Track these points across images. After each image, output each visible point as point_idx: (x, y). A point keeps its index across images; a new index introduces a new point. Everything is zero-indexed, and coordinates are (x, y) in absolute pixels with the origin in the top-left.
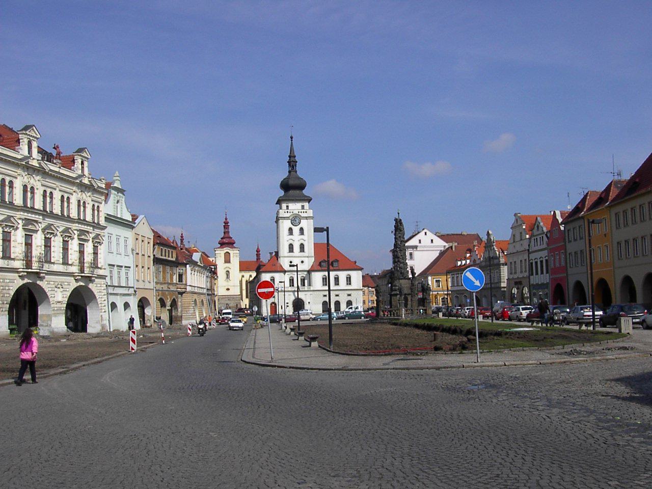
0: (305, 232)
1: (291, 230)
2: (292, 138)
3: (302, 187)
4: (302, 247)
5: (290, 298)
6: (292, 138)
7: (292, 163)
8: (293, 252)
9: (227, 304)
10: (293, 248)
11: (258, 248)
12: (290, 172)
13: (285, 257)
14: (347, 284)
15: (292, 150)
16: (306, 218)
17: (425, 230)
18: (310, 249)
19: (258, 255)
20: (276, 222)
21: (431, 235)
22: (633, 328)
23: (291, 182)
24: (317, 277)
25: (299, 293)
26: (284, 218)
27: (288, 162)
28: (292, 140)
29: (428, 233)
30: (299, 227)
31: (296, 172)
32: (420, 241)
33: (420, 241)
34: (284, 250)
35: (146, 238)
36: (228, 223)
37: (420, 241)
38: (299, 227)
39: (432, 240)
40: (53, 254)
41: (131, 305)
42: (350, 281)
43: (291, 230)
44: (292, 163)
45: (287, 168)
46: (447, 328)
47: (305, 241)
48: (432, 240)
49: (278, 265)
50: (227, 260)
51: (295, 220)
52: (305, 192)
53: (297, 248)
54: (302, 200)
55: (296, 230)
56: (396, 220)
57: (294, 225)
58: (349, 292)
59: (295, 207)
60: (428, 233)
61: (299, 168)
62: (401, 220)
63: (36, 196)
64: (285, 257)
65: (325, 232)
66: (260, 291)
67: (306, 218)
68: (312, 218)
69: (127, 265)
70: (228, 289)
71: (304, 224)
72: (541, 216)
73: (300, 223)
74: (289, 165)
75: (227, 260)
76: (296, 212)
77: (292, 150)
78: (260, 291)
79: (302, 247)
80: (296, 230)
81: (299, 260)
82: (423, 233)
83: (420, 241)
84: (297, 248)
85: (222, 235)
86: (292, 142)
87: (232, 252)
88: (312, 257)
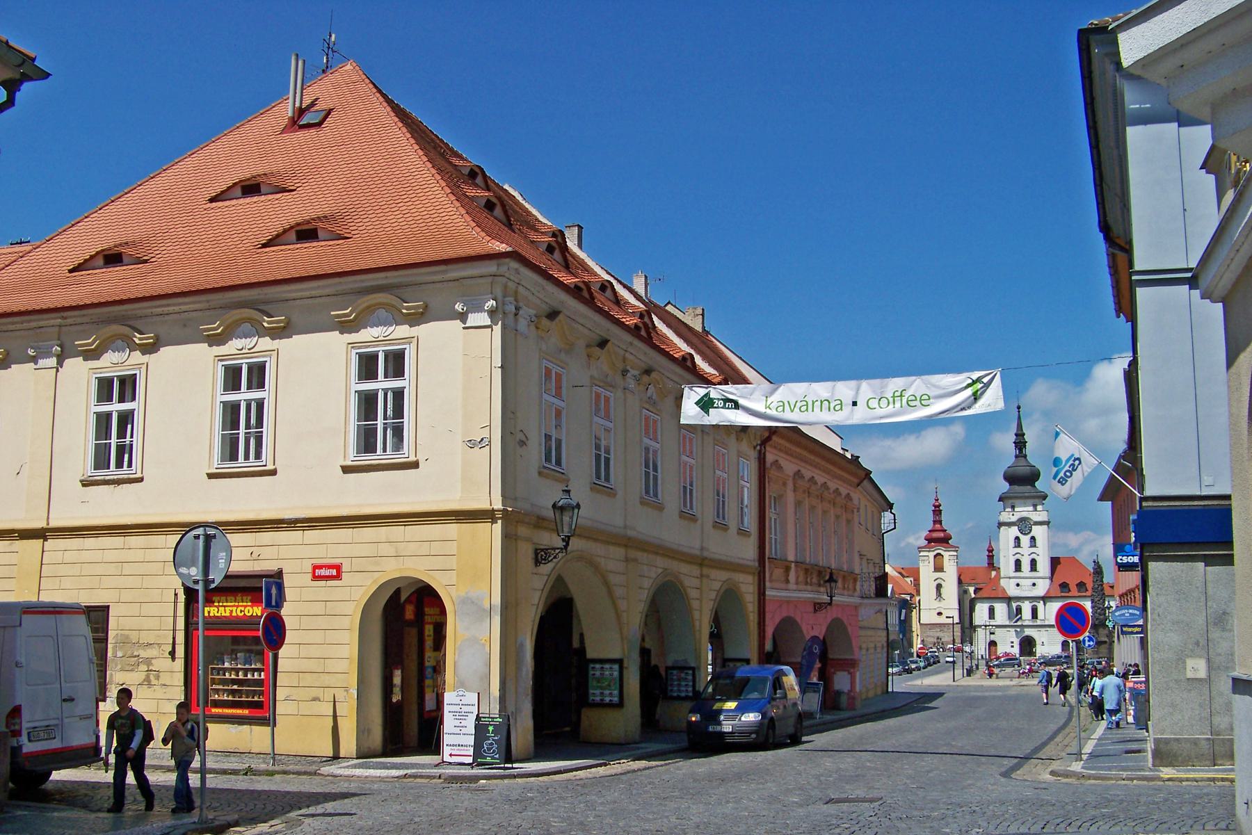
1: (1017, 538)
2: (1019, 408)
4: (1033, 564)
6: (1019, 408)
12: (1016, 457)
16: (1037, 523)
18: (1044, 567)
19: (991, 557)
22: (110, 381)
23: (1023, 470)
25: (269, 750)
26: (1010, 524)
31: (1025, 456)
34: (1006, 564)
43: (1017, 538)
50: (939, 568)
51: (1024, 525)
53: (1026, 566)
54: (1116, 104)
55: (1025, 540)
59: (1024, 511)
61: (1029, 449)
67: (1037, 523)
68: (1047, 523)
69: (612, 462)
70: (940, 614)
75: (939, 568)
76: (1025, 515)
79: (1033, 564)
80: (1025, 540)
81: (1030, 582)
84: (1026, 566)
85: (930, 526)
87: (946, 555)
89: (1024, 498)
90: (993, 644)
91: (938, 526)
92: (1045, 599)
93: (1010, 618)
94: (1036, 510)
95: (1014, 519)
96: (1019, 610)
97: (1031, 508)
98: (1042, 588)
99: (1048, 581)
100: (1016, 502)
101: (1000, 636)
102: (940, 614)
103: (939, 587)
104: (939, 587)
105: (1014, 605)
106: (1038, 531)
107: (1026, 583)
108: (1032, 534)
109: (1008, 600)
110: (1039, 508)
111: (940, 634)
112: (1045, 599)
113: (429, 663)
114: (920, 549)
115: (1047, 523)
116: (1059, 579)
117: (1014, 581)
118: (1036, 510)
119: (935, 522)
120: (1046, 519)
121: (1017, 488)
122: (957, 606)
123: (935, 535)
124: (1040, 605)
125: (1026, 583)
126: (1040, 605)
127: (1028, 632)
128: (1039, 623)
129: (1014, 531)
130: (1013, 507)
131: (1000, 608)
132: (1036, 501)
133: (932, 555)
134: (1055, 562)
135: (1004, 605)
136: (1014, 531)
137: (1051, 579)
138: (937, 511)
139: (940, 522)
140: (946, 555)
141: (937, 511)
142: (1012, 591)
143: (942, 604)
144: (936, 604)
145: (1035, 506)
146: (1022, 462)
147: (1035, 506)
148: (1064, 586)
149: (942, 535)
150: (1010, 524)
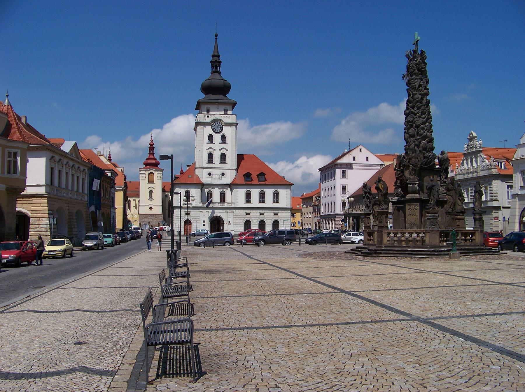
0: (228, 140)
1: (211, 137)
2: (216, 35)
3: (224, 89)
4: (223, 157)
5: (206, 215)
6: (216, 35)
7: (216, 64)
9: (149, 223)
11: (182, 170)
13: (203, 168)
15: (216, 49)
17: (361, 147)
18: (231, 160)
20: (194, 129)
21: (366, 153)
23: (217, 82)
24: (241, 193)
27: (211, 62)
28: (216, 39)
31: (219, 73)
32: (354, 159)
33: (354, 159)
34: (201, 159)
36: (153, 144)
37: (354, 158)
39: (367, 158)
43: (211, 137)
44: (216, 64)
45: (209, 68)
46: (54, 221)
47: (227, 150)
48: (367, 158)
49: (195, 177)
50: (151, 181)
52: (230, 96)
53: (217, 158)
55: (217, 138)
57: (214, 132)
59: (217, 114)
60: (363, 149)
61: (222, 69)
62: (422, 52)
64: (203, 168)
70: (151, 208)
73: (222, 130)
74: (212, 66)
75: (151, 181)
76: (218, 117)
77: (216, 49)
79: (223, 157)
80: (217, 138)
81: (220, 172)
82: (358, 149)
83: (354, 158)
84: (217, 158)
86: (216, 43)
87: (156, 173)
89: (218, 104)
90: (188, 223)
91: (152, 156)
92: (232, 186)
93: (202, 201)
94: (226, 113)
95: (208, 120)
96: (210, 195)
97: (223, 113)
98: (230, 177)
99: (234, 172)
100: (211, 107)
101: (194, 216)
102: (151, 208)
103: (151, 192)
104: (151, 192)
105: (206, 190)
106: (227, 131)
107: (216, 173)
108: (223, 132)
109: (202, 186)
110: (229, 112)
111: (151, 221)
112: (232, 186)
113: (188, 228)
114: (140, 170)
116: (244, 170)
117: (206, 171)
118: (226, 113)
119: (150, 154)
121: (211, 96)
122: (161, 204)
123: (150, 161)
124: (228, 191)
125: (216, 173)
126: (228, 191)
127: (218, 213)
128: (226, 205)
129: (208, 130)
130: (208, 112)
131: (195, 192)
132: (227, 107)
133: (147, 173)
134: (240, 158)
135: (198, 190)
136: (208, 130)
137: (237, 170)
139: (153, 154)
140: (156, 173)
142: (205, 179)
143: (153, 203)
144: (149, 202)
145: (226, 111)
146: (216, 76)
147: (226, 111)
148: (248, 176)
149: (154, 161)
150: (205, 124)
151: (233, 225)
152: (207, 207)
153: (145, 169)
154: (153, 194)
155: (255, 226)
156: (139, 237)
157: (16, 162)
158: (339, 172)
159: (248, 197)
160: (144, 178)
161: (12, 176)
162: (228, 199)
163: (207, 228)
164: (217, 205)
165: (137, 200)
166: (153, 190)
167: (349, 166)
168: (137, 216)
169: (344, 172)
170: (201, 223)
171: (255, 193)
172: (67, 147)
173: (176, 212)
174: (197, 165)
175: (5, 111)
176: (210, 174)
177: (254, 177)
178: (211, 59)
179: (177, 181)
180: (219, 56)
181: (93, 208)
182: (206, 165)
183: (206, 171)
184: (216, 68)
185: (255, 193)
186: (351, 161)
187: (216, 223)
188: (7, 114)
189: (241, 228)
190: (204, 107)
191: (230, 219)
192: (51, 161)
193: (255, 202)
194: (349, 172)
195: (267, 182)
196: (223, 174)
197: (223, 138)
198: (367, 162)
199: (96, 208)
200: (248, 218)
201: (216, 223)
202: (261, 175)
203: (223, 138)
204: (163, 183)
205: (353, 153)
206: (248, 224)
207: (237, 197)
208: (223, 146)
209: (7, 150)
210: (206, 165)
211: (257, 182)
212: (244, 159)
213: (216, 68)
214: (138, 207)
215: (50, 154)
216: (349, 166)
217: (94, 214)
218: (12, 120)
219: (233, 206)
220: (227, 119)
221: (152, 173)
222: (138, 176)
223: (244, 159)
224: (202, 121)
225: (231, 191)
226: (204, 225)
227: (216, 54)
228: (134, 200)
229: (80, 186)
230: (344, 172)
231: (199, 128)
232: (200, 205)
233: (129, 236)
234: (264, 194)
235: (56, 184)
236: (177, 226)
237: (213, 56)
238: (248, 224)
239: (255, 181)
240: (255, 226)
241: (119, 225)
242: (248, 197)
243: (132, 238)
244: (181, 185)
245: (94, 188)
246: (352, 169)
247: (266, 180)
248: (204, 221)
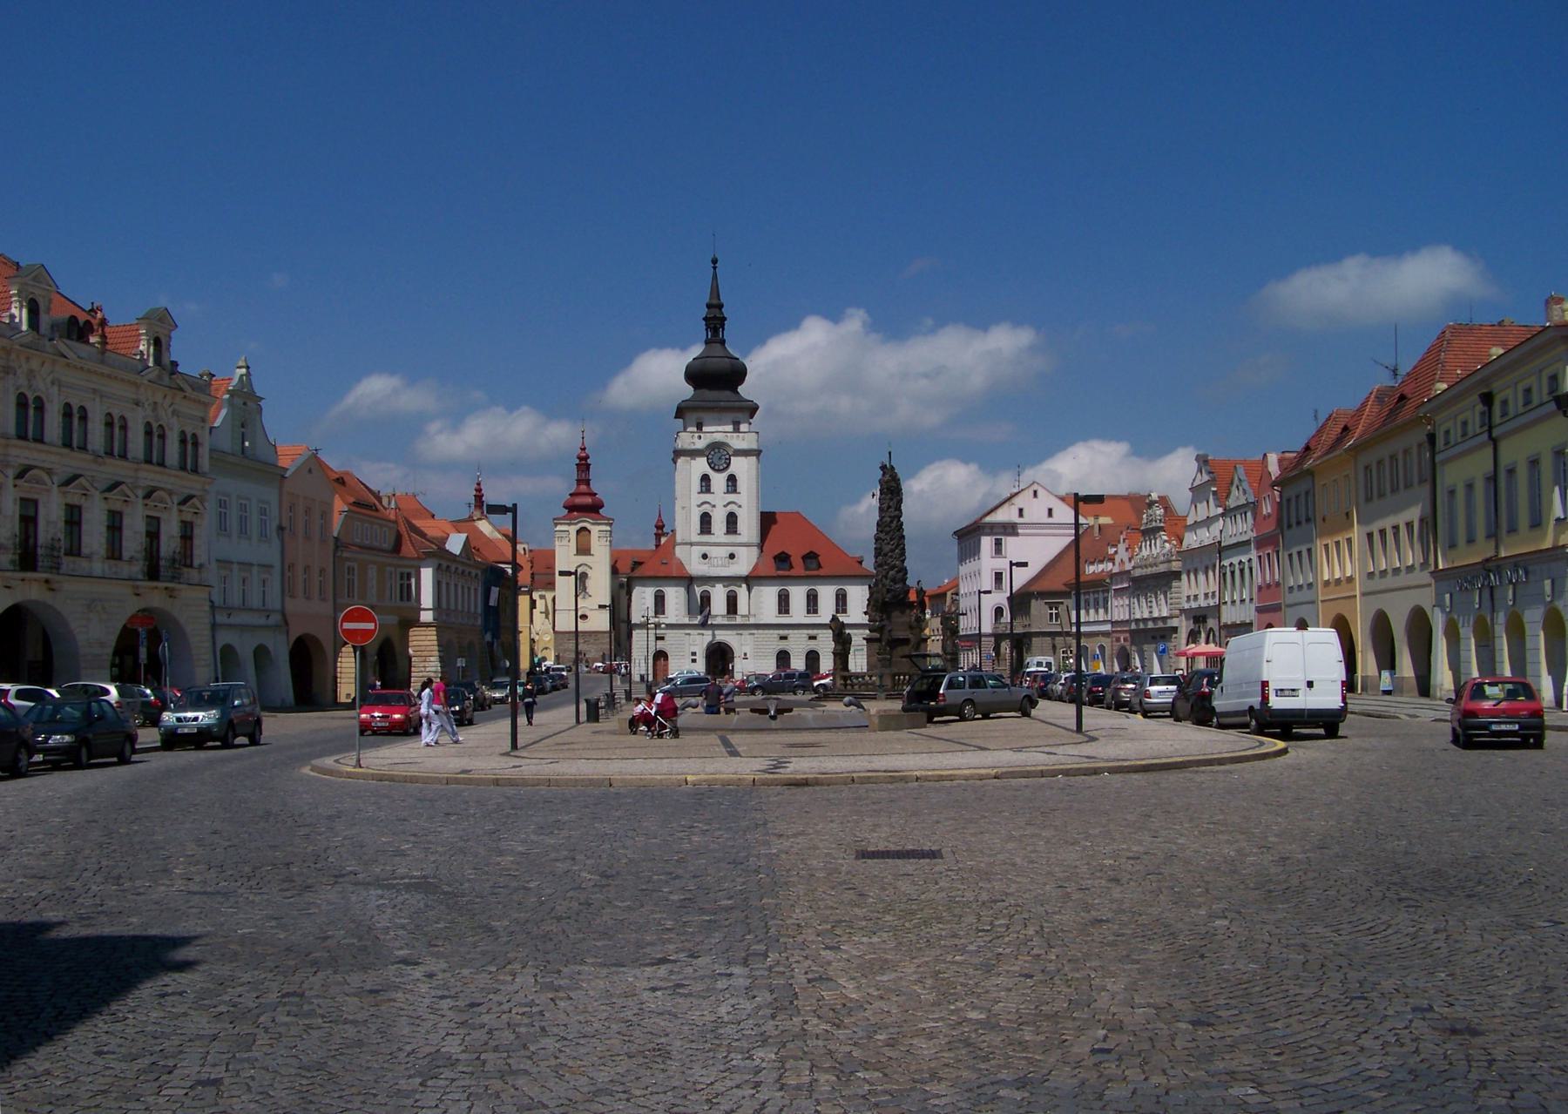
1: (705, 479)
2: (715, 261)
4: (732, 520)
5: (700, 642)
6: (715, 261)
7: (715, 323)
8: (709, 532)
10: (709, 523)
13: (691, 544)
14: (808, 612)
15: (715, 291)
17: (1035, 487)
18: (749, 527)
24: (767, 596)
29: (1041, 492)
30: (724, 475)
31: (723, 342)
34: (686, 525)
35: (255, 570)
36: (587, 457)
37: (1021, 510)
38: (724, 475)
39: (1050, 511)
40: (196, 552)
41: (120, 626)
42: (816, 604)
43: (705, 479)
44: (715, 323)
48: (1050, 511)
50: (583, 549)
53: (719, 524)
55: (719, 480)
56: (883, 468)
58: (811, 632)
59: (717, 431)
61: (729, 332)
63: (168, 442)
64: (691, 544)
65: (510, 515)
66: (347, 626)
68: (757, 453)
71: (740, 466)
72: (1244, 463)
75: (583, 549)
76: (719, 437)
77: (715, 291)
78: (347, 626)
79: (732, 520)
80: (719, 480)
83: (1021, 510)
84: (719, 524)
86: (715, 277)
87: (595, 530)
88: (562, 573)
90: (661, 656)
91: (583, 488)
92: (750, 580)
94: (737, 430)
95: (700, 444)
96: (706, 599)
97: (730, 428)
98: (746, 562)
99: (755, 551)
100: (705, 416)
105: (698, 590)
106: (740, 466)
108: (731, 470)
109: (689, 581)
110: (744, 427)
112: (750, 580)
114: (557, 521)
115: (757, 453)
116: (774, 547)
117: (697, 551)
118: (737, 430)
119: (579, 482)
120: (754, 446)
124: (742, 592)
126: (742, 592)
127: (723, 636)
128: (739, 620)
129: (701, 465)
130: (699, 427)
132: (739, 416)
133: (573, 529)
134: (767, 521)
135: (682, 590)
137: (761, 546)
138: (583, 465)
139: (587, 482)
140: (595, 530)
141: (583, 465)
142: (695, 567)
145: (736, 425)
147: (736, 425)
148: (782, 559)
149: (588, 500)
150: (693, 454)
151: (753, 659)
152: (704, 625)
153: (568, 519)
154: (589, 583)
155: (798, 664)
156: (565, 686)
157: (409, 586)
158: (987, 542)
159: (784, 604)
160: (565, 542)
161: (405, 604)
162: (742, 607)
163: (700, 668)
164: (719, 621)
165: (549, 595)
166: (589, 572)
167: (1010, 529)
168: (548, 638)
169: (998, 543)
170: (687, 660)
171: (798, 594)
172: (455, 544)
173: (638, 637)
174: (679, 539)
175: (392, 517)
176: (705, 556)
177: (796, 560)
178: (704, 311)
179: (637, 573)
180: (721, 306)
181: (488, 637)
182: (696, 538)
183: (697, 551)
184: (715, 331)
185: (798, 594)
186: (1015, 518)
187: (719, 657)
188: (396, 522)
189: (769, 667)
190: (692, 417)
191: (747, 649)
192: (438, 570)
193: (798, 612)
194: (1009, 542)
195: (821, 572)
196: (732, 556)
197: (732, 479)
198: (1050, 520)
199: (494, 636)
200: (783, 645)
201: (719, 657)
202: (811, 557)
203: (732, 479)
204: (612, 555)
205: (1019, 502)
206: (783, 658)
207: (762, 603)
208: (732, 497)
209: (400, 570)
210: (696, 538)
211: (803, 573)
212: (775, 522)
213: (715, 331)
214: (551, 613)
215: (436, 562)
216: (1010, 529)
217: (491, 645)
218: (403, 529)
219: (752, 621)
220: (737, 442)
221: (584, 529)
222: (552, 537)
223: (775, 522)
224: (687, 447)
225: (749, 591)
226: (694, 661)
227: (715, 302)
228: (542, 597)
229: (471, 601)
230: (998, 543)
231: (681, 461)
232: (686, 621)
233: (548, 684)
234: (816, 597)
235: (444, 605)
236: (640, 665)
237: (709, 306)
238: (783, 658)
239: (799, 569)
240: (798, 664)
241: (525, 664)
242: (784, 604)
243: (555, 688)
244: (647, 580)
245: (492, 603)
246: (1017, 534)
247: (820, 566)
248: (694, 654)
